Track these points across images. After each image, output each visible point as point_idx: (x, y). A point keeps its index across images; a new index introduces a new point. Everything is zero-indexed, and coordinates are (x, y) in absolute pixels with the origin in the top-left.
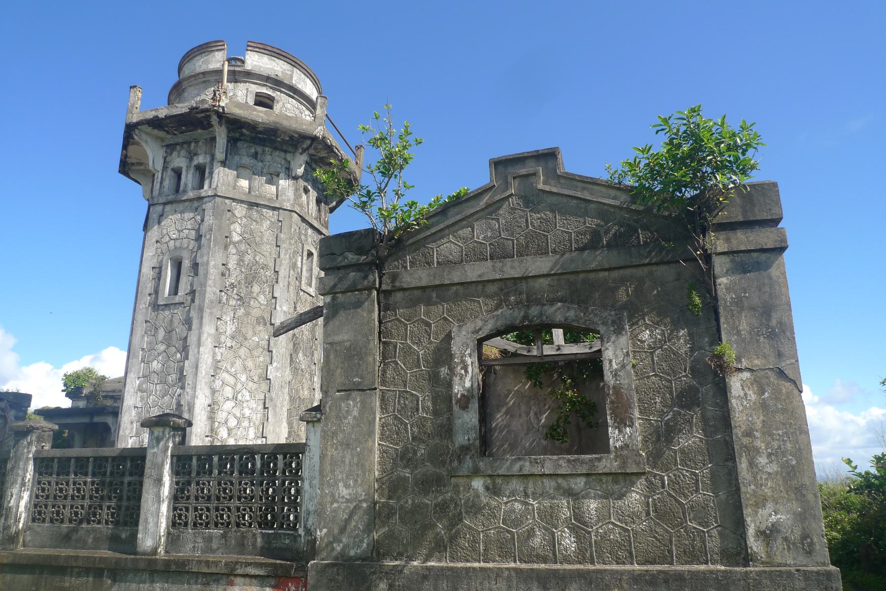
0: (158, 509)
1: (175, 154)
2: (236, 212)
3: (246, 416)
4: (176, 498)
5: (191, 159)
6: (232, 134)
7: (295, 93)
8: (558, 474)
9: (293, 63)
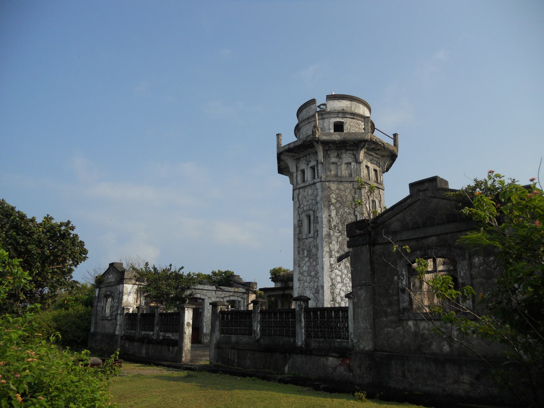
0: (301, 331)
1: (300, 163)
2: (332, 187)
3: (349, 291)
4: (307, 327)
5: (308, 164)
6: (325, 148)
7: (354, 115)
8: (353, 314)
9: (351, 100)
